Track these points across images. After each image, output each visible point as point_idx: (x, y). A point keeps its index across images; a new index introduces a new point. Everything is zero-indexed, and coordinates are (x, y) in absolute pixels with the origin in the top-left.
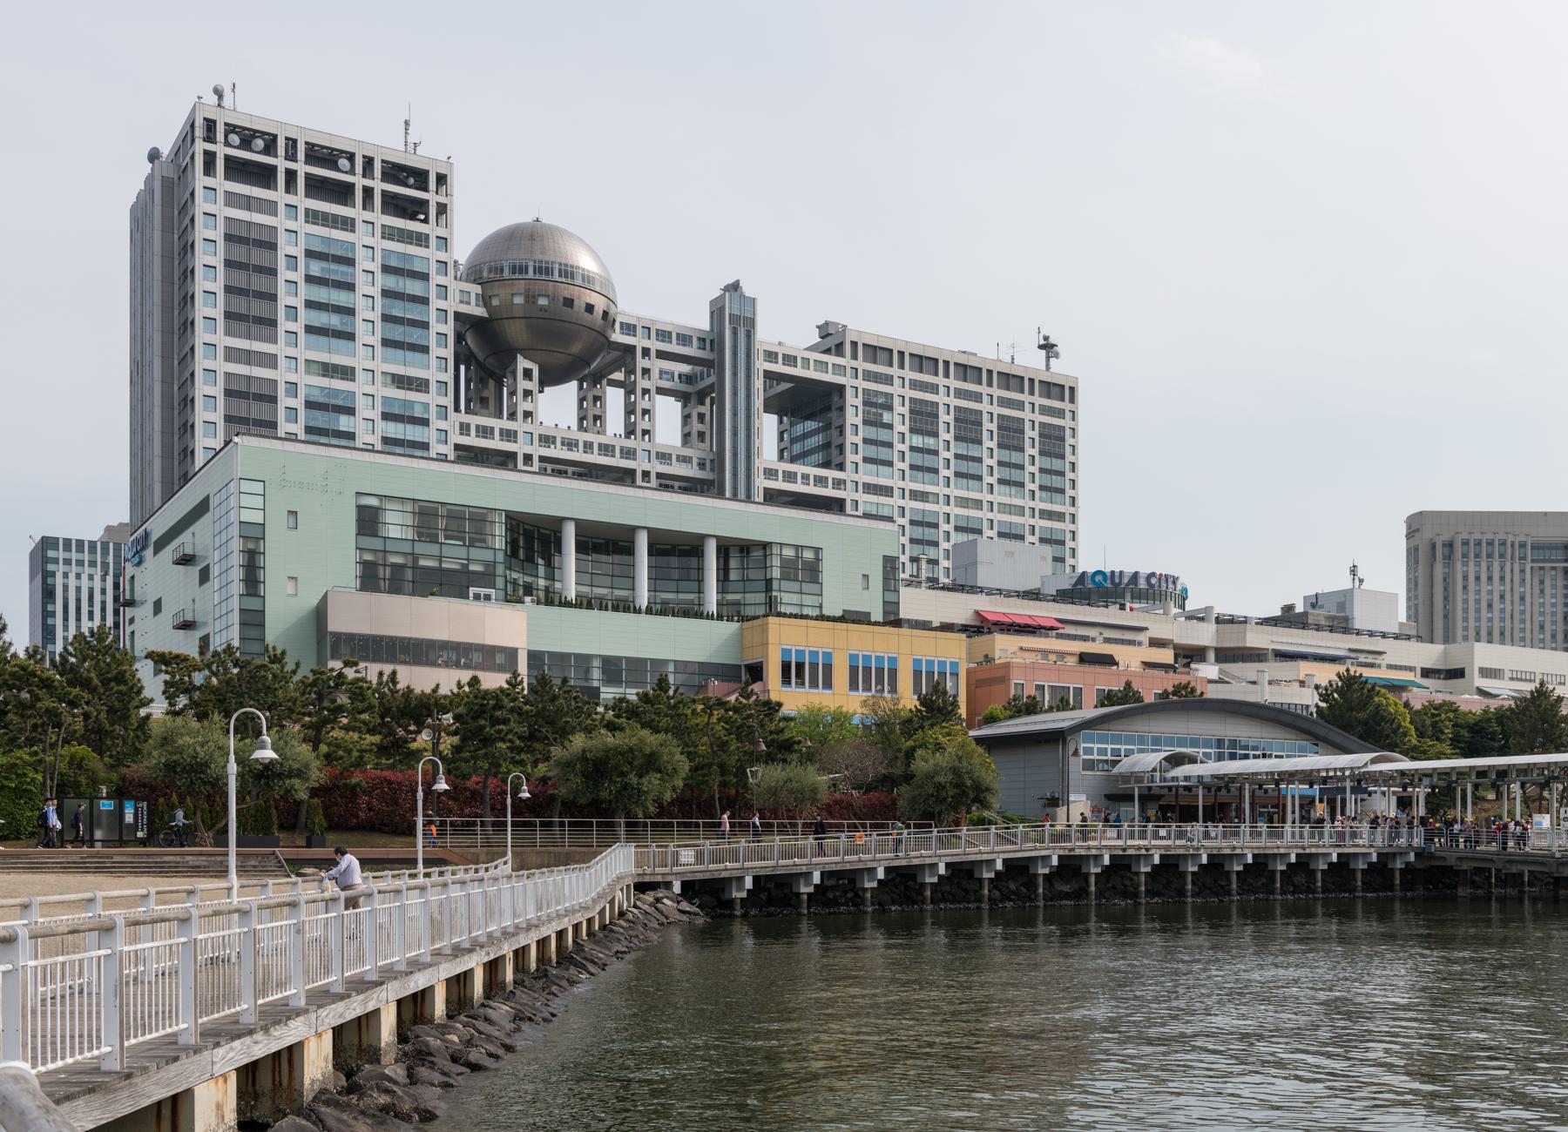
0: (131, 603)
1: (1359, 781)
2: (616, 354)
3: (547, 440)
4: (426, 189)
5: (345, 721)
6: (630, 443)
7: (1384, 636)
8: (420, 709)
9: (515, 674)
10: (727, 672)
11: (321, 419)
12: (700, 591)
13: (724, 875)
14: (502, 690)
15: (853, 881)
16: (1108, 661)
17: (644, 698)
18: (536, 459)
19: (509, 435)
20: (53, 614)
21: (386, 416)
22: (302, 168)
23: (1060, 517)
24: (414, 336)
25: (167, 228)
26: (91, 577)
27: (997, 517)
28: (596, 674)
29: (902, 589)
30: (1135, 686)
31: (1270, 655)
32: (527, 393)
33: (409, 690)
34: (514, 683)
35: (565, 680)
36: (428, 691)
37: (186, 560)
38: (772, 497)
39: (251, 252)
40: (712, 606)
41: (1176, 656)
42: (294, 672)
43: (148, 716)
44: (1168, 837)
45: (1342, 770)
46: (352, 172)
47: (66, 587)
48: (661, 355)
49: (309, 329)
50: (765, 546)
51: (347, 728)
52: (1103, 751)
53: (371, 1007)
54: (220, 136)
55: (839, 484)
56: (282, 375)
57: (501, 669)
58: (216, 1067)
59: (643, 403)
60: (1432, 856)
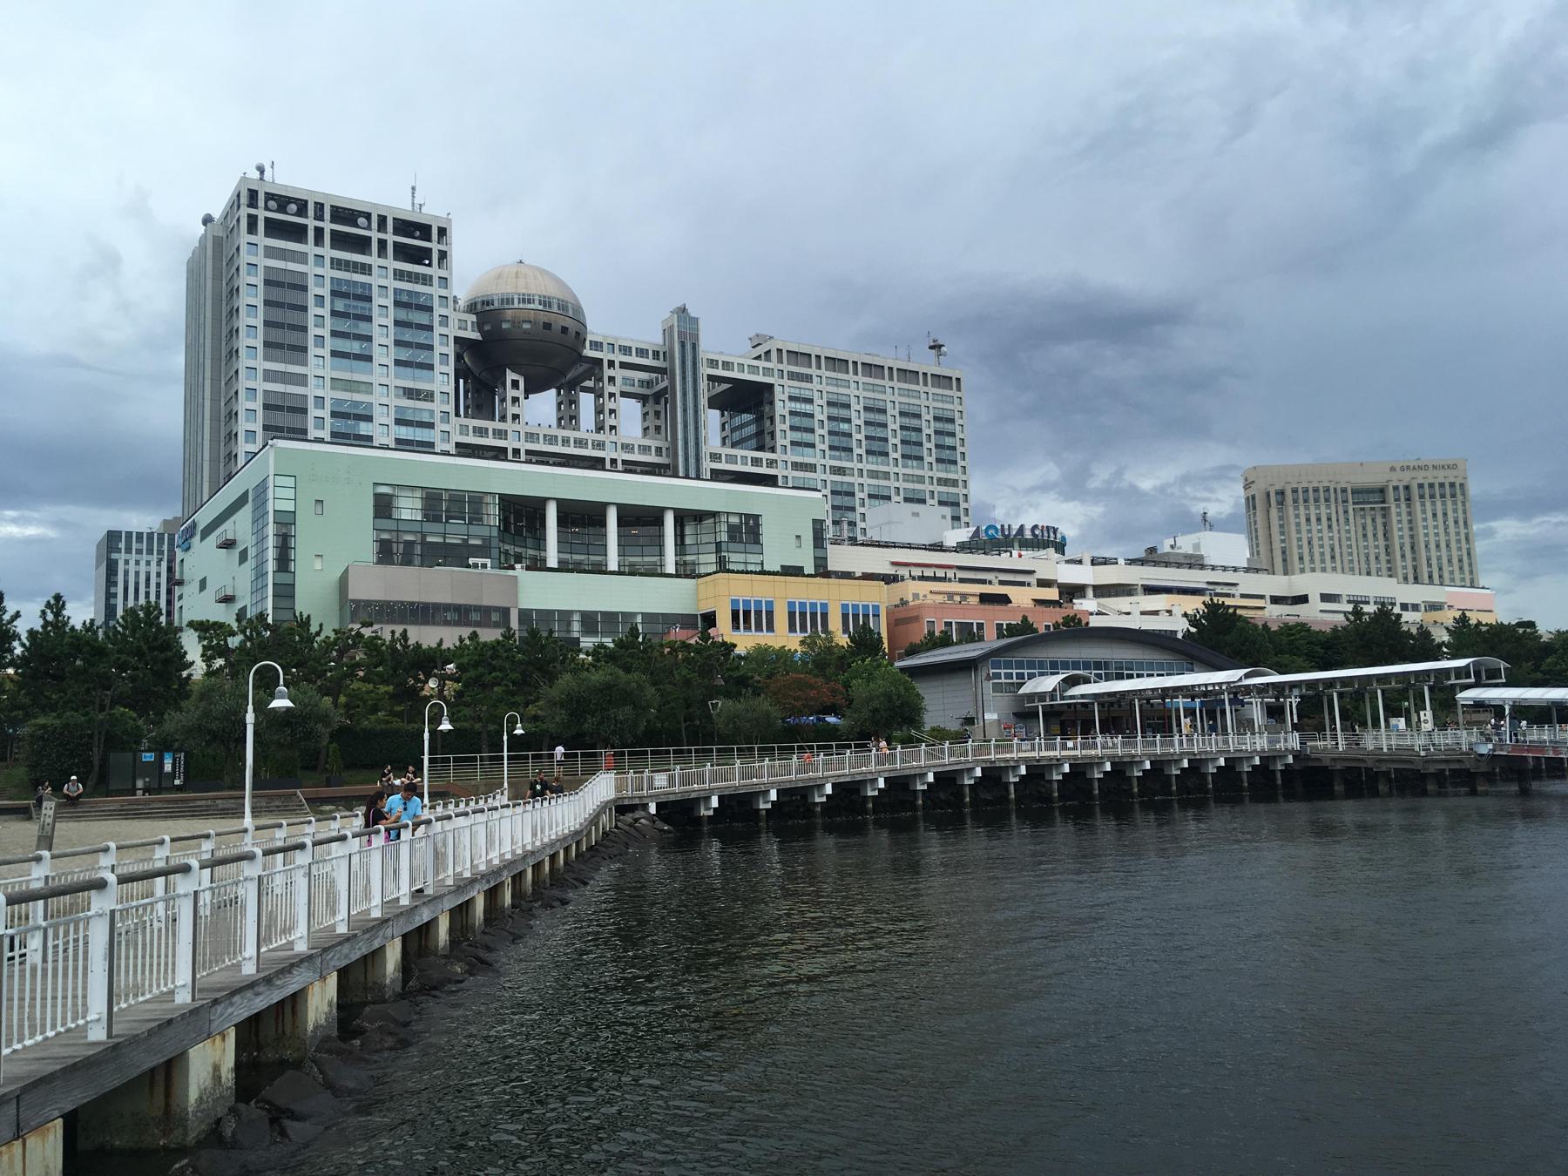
0: (180, 583)
1: (1235, 694)
2: (585, 366)
3: (531, 437)
4: (429, 240)
5: (361, 674)
6: (600, 437)
7: (1235, 569)
8: (429, 661)
9: (509, 629)
10: (687, 621)
11: (343, 426)
12: (661, 554)
13: (693, 795)
14: (498, 642)
15: (805, 797)
16: (1004, 600)
17: (620, 644)
18: (523, 453)
19: (501, 434)
20: (115, 595)
21: (398, 422)
22: (328, 226)
23: (954, 483)
24: (422, 357)
25: (217, 276)
26: (148, 563)
27: (902, 485)
28: (576, 627)
29: (829, 547)
30: (1030, 620)
31: (1140, 589)
32: (515, 400)
33: (418, 645)
34: (508, 635)
35: (551, 632)
36: (434, 645)
37: (228, 545)
38: (717, 475)
39: (285, 295)
40: (670, 568)
41: (1061, 594)
42: (318, 634)
43: (190, 675)
44: (1075, 748)
45: (1220, 684)
46: (369, 228)
47: (126, 573)
48: (624, 365)
49: (334, 354)
50: (714, 514)
51: (363, 680)
52: (1009, 676)
53: (376, 945)
54: (261, 203)
55: (771, 463)
56: (312, 391)
57: (496, 625)
58: (213, 1026)
59: (609, 405)
60: (1308, 758)
